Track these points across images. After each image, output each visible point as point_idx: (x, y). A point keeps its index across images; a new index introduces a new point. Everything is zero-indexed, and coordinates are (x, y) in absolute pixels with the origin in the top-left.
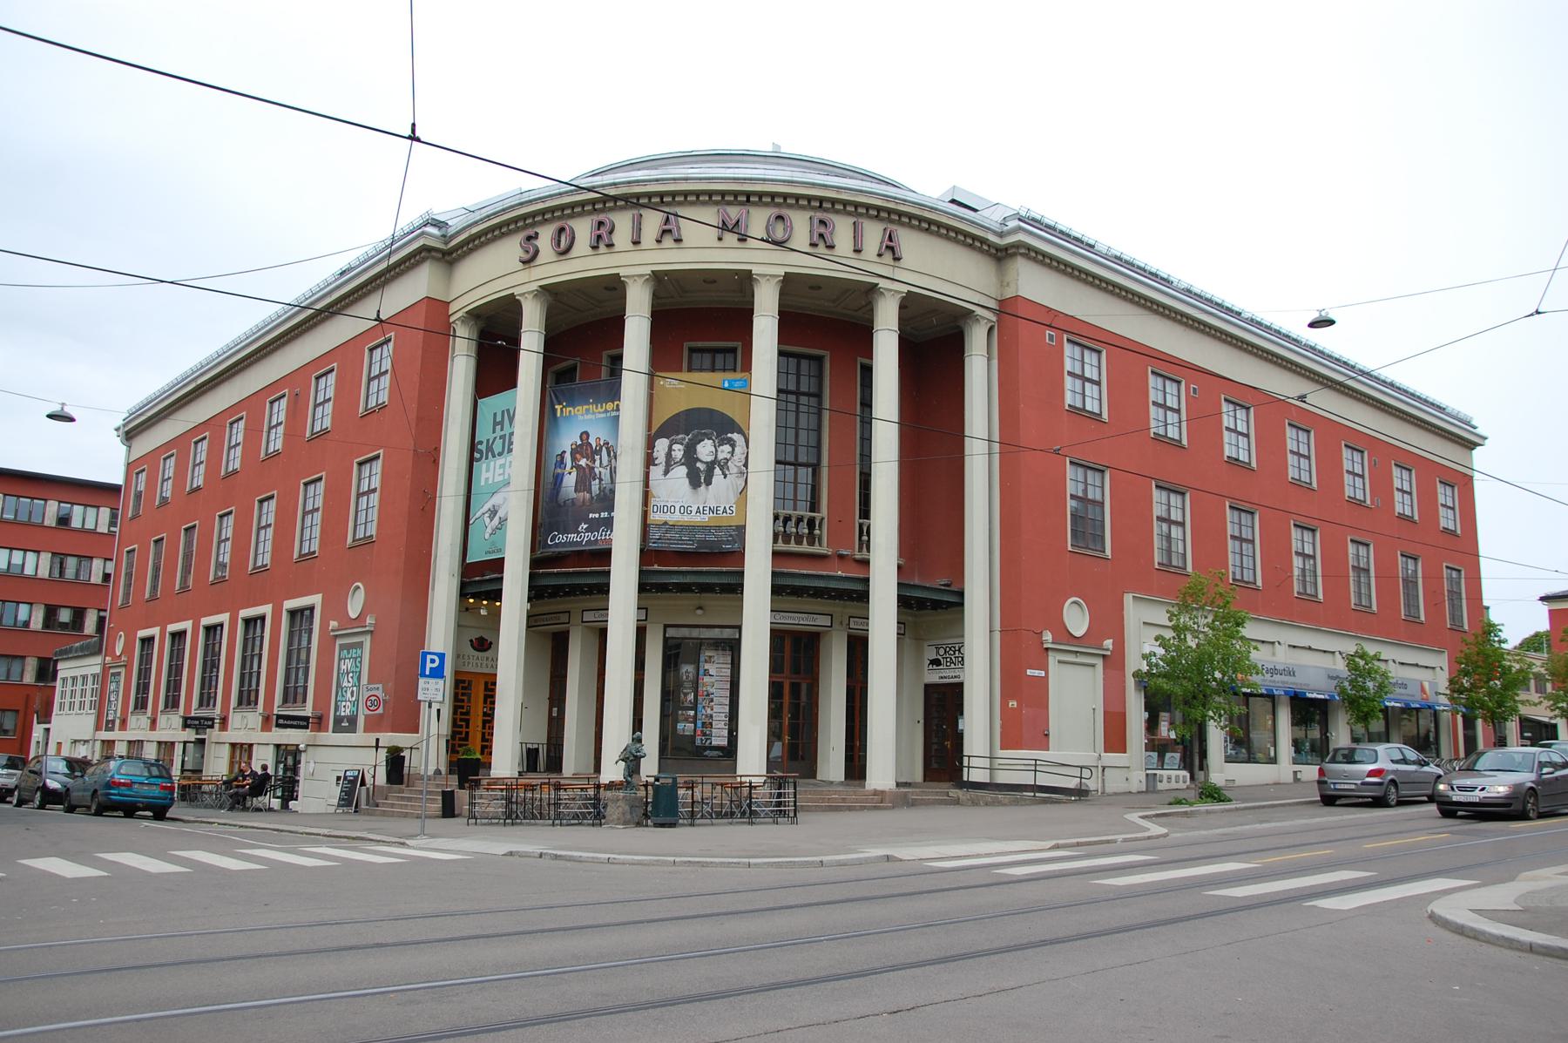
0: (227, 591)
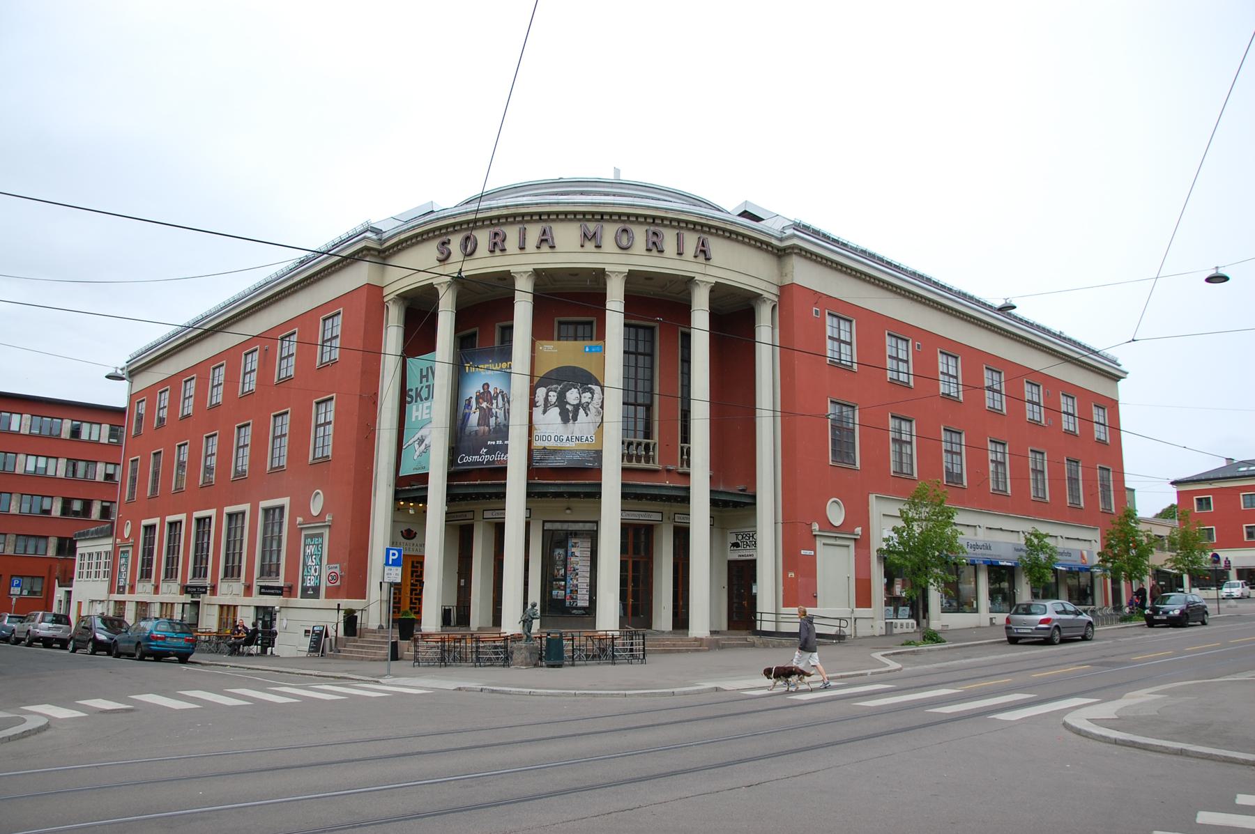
0: (212, 492)
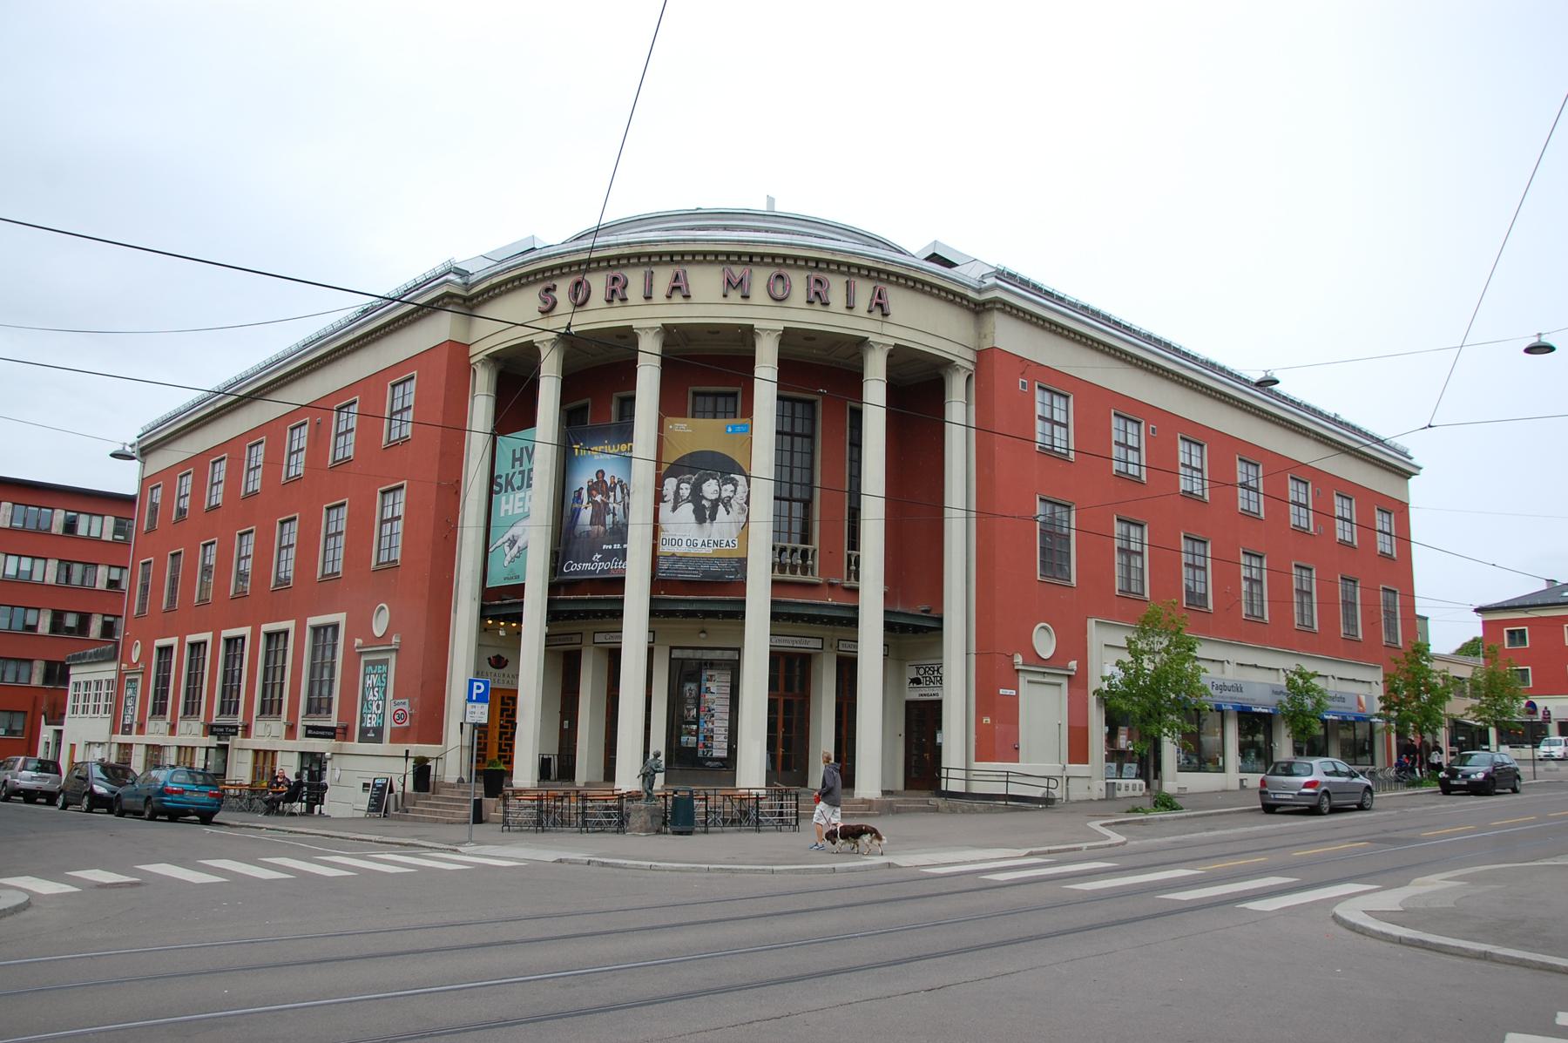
0: (245, 606)
